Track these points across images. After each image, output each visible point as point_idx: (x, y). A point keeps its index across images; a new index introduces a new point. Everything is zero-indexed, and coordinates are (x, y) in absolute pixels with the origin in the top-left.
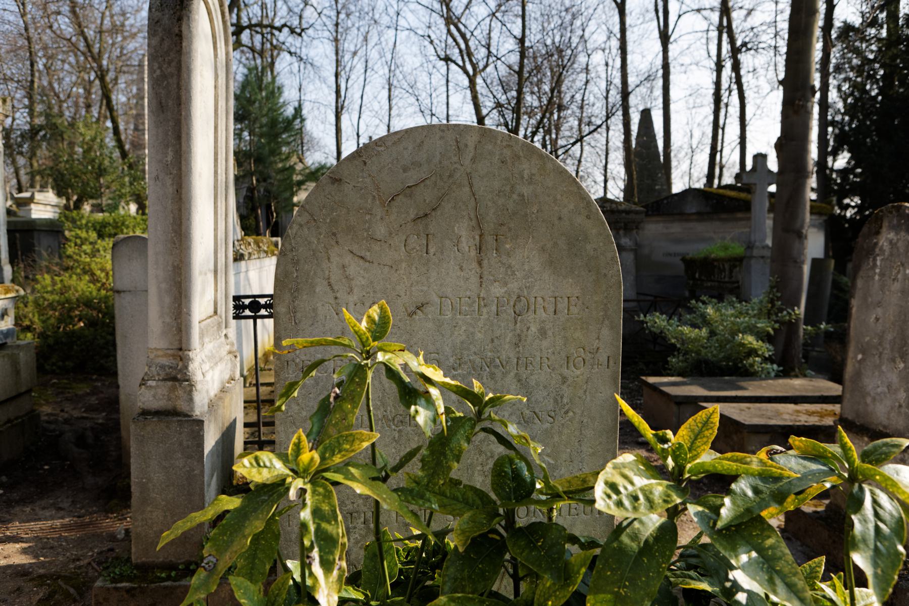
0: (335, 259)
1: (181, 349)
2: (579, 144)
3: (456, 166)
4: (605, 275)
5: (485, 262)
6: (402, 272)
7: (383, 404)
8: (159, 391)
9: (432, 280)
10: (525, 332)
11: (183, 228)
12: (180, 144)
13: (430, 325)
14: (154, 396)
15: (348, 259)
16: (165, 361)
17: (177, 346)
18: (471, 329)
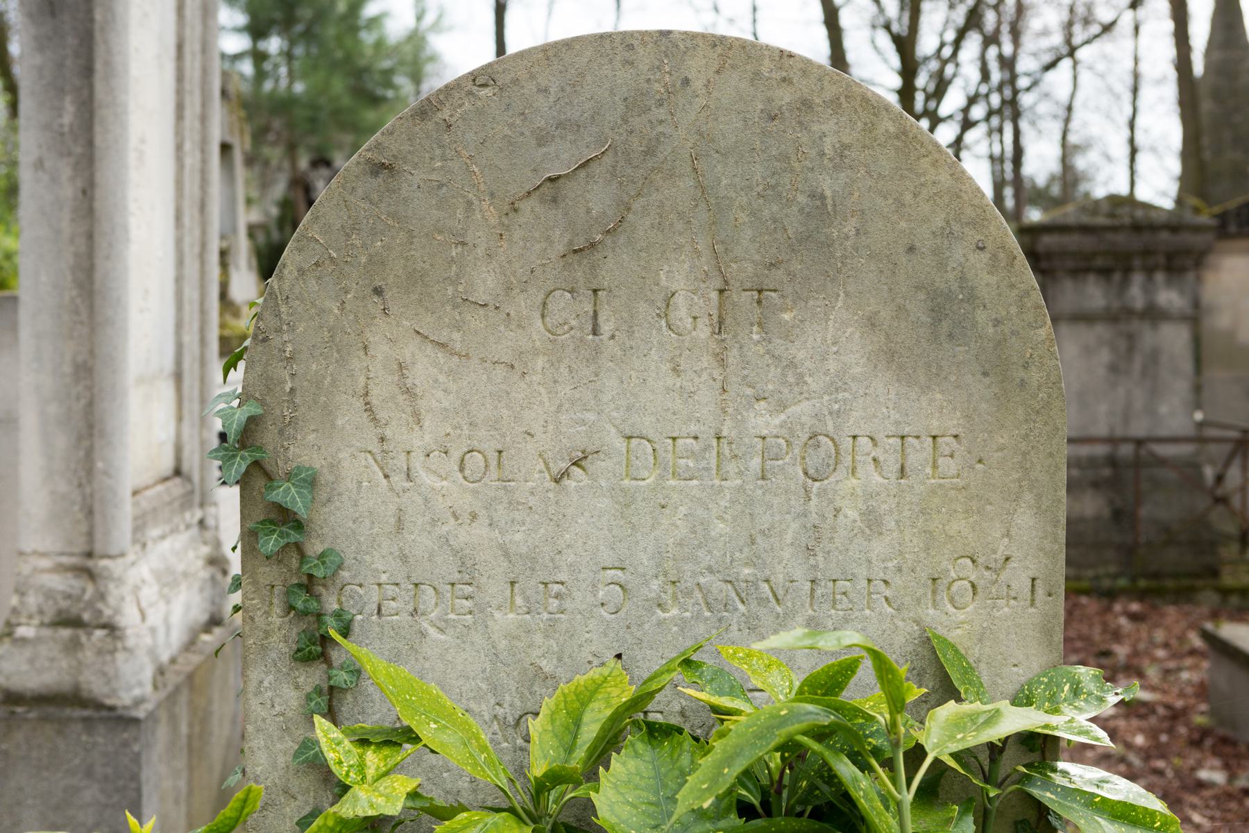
0: (381, 350)
1: (89, 555)
2: (1066, 64)
3: (660, 129)
4: (1023, 383)
5: (733, 357)
6: (536, 378)
7: (494, 689)
8: (43, 650)
9: (606, 398)
10: (830, 520)
11: (98, 276)
12: (91, 87)
13: (604, 503)
14: (31, 661)
15: (409, 349)
16: (58, 582)
17: (85, 548)
18: (700, 512)
